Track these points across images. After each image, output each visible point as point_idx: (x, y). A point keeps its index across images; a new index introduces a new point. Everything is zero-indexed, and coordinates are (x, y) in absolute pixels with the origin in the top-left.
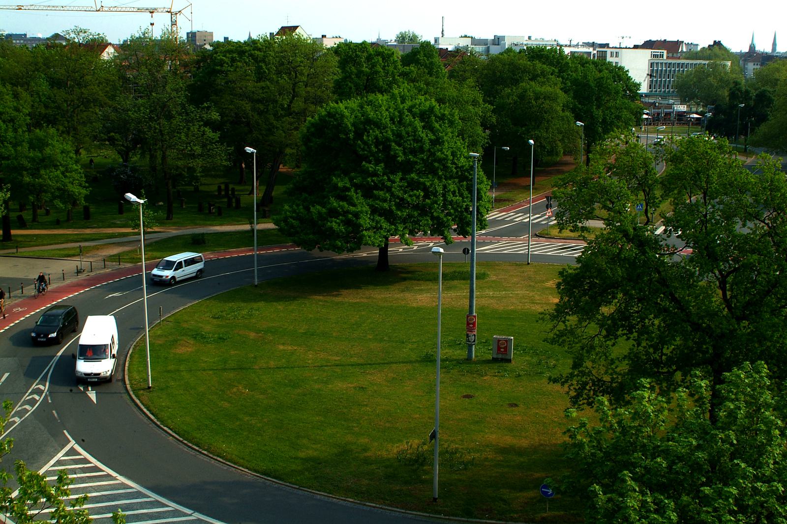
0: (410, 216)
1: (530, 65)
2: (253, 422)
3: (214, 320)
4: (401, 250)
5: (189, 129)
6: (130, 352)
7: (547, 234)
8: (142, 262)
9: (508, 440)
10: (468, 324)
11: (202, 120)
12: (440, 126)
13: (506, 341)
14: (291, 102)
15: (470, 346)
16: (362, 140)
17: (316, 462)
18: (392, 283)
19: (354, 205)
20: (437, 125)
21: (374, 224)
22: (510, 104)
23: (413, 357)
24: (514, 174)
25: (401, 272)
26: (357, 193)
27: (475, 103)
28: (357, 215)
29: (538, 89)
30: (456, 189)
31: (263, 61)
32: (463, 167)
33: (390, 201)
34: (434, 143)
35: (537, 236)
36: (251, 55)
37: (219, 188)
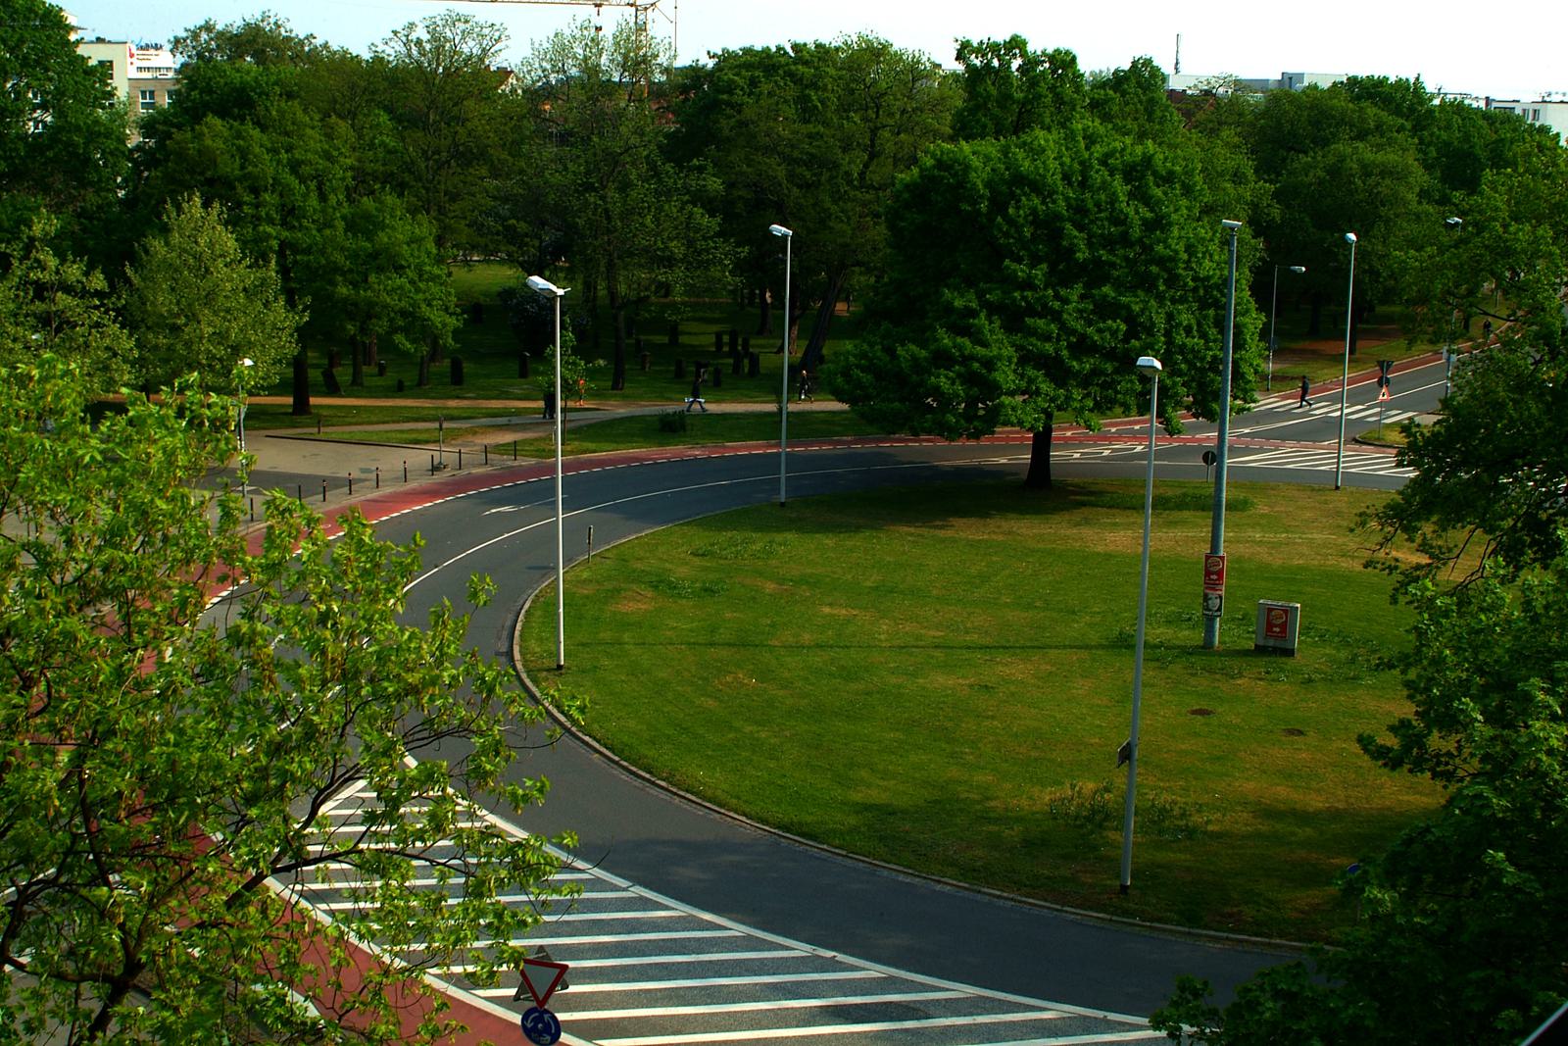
0: (1096, 371)
1: (1353, 111)
2: (763, 735)
3: (696, 559)
4: (1077, 456)
5: (660, 209)
6: (527, 606)
7: (1378, 439)
8: (556, 456)
9: (1283, 793)
10: (1208, 573)
11: (688, 192)
12: (1165, 193)
13: (1286, 612)
14: (866, 166)
15: (1211, 620)
16: (1005, 216)
17: (886, 811)
18: (1055, 510)
19: (985, 345)
20: (1158, 192)
21: (1024, 384)
22: (1311, 184)
23: (1094, 637)
24: (1314, 332)
25: (1074, 493)
26: (991, 322)
27: (1237, 178)
28: (989, 364)
29: (1369, 156)
30: (1193, 322)
31: (814, 86)
32: (1208, 278)
33: (1058, 340)
34: (1150, 226)
35: (1357, 441)
36: (791, 75)
37: (719, 343)
